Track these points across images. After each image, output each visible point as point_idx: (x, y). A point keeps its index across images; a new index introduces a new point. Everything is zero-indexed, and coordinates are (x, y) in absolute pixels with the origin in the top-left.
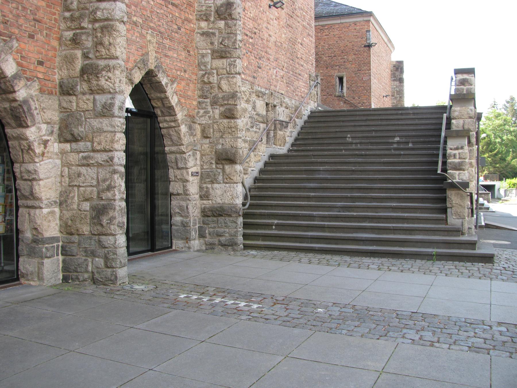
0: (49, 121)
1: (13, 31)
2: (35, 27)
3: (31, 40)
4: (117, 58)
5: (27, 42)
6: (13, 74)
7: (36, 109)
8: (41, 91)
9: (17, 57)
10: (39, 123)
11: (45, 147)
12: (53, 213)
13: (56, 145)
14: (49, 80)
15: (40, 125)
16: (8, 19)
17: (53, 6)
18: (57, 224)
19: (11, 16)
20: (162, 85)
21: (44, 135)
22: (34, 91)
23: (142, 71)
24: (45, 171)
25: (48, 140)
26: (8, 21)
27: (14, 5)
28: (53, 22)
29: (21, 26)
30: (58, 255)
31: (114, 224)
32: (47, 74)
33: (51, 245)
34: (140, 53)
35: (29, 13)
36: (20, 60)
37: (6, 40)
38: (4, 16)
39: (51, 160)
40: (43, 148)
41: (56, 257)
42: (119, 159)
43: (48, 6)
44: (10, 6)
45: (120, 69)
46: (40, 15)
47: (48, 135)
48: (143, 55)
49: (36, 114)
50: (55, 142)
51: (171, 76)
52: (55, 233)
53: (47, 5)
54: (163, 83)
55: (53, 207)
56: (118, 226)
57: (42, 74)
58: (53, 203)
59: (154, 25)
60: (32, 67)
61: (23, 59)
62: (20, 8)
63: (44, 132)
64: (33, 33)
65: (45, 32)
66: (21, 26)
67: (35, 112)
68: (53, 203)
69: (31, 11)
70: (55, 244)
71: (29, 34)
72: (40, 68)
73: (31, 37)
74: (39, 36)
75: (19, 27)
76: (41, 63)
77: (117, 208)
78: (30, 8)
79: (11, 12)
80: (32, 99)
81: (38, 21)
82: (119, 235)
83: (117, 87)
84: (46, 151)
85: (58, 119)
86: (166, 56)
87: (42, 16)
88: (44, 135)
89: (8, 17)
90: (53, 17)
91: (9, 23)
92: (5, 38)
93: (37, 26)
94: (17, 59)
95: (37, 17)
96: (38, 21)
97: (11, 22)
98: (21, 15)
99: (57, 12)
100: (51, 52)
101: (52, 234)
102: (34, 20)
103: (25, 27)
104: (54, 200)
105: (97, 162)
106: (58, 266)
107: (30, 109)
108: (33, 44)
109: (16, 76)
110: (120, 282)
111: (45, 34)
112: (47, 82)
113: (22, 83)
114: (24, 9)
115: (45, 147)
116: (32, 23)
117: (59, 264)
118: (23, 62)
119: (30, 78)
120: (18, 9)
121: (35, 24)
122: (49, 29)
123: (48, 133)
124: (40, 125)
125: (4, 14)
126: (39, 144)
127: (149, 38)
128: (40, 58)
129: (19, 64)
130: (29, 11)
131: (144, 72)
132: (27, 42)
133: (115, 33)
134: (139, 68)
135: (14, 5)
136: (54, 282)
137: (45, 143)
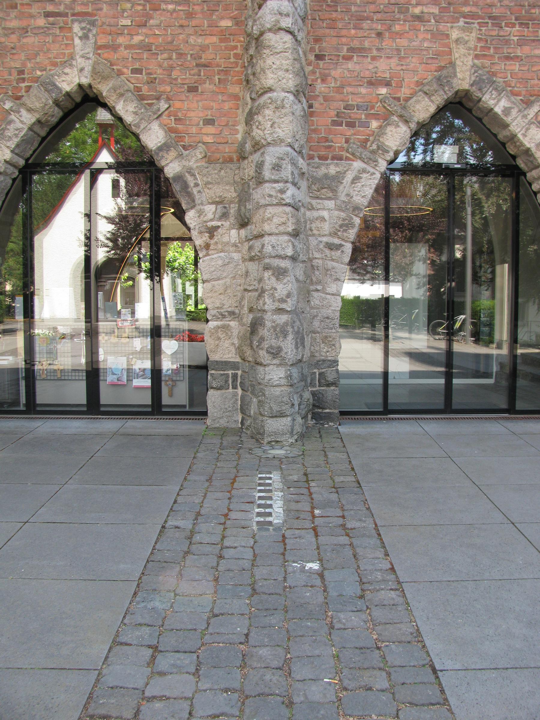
0: (217, 199)
1: (162, 89)
2: (200, 75)
3: (191, 95)
4: (270, 90)
5: (184, 98)
6: (159, 144)
7: (197, 185)
8: (209, 159)
9: (169, 121)
10: (202, 204)
11: (212, 237)
12: (225, 328)
13: (234, 232)
14: (226, 143)
15: (202, 207)
16: (155, 76)
17: (232, 37)
18: (233, 344)
19: (159, 72)
20: (496, 114)
21: (211, 220)
22: (197, 161)
23: (433, 98)
24: (213, 269)
25: (218, 227)
26: (155, 79)
27: (165, 56)
28: (232, 60)
29: (176, 79)
30: (235, 387)
31: (262, 349)
32: (222, 135)
33: (222, 372)
34: (434, 66)
35: (189, 58)
36: (173, 125)
37: (152, 104)
38: (150, 74)
39: (222, 254)
40: (207, 238)
41: (231, 390)
42: (273, 247)
43: (221, 41)
44: (159, 59)
45: (272, 107)
46: (206, 57)
47: (220, 219)
48: (441, 68)
49: (195, 193)
50: (233, 229)
51: (523, 93)
52: (230, 356)
53: (220, 39)
54: (498, 110)
55: (227, 319)
56: (268, 352)
57: (212, 137)
58: (226, 314)
59: (474, 9)
60: (194, 130)
61: (177, 122)
62: (174, 57)
63: (210, 216)
64: (196, 85)
65: (217, 77)
66: (176, 79)
67: (195, 191)
68: (226, 314)
69: (191, 55)
70: (230, 372)
71: (188, 87)
72: (210, 129)
73: (193, 89)
74: (207, 85)
75: (172, 82)
76: (209, 122)
77: (268, 324)
78: (191, 52)
79: (160, 66)
80: (189, 173)
81: (205, 66)
82: (271, 367)
83: (267, 136)
84: (212, 242)
85: (235, 195)
86: (508, 58)
87: (213, 56)
88: (211, 220)
89: (155, 73)
90: (232, 53)
91: (157, 81)
92: (150, 102)
93: (202, 74)
94: (168, 124)
95: (203, 60)
96: (205, 66)
97: (160, 79)
98: (175, 66)
99: (239, 44)
100: (227, 103)
101: (226, 356)
102: (197, 65)
103: (182, 79)
104: (229, 310)
105: (477, 272)
106: (235, 402)
107: (185, 186)
108: (195, 98)
109: (165, 147)
110: (270, 440)
111: (217, 81)
112: (221, 147)
113: (173, 154)
114: (181, 55)
115: (212, 237)
116: (196, 71)
117: (237, 400)
118: (178, 126)
119: (190, 146)
120: (170, 58)
121: (200, 71)
122: (226, 72)
123: (217, 216)
124: (202, 207)
125: (150, 71)
126: (201, 233)
127: (455, 34)
128: (209, 115)
129: (171, 130)
130: (189, 56)
131: (439, 99)
132: (184, 98)
133: (265, 51)
134: (426, 93)
135: (165, 56)
136: (225, 424)
137: (212, 231)
